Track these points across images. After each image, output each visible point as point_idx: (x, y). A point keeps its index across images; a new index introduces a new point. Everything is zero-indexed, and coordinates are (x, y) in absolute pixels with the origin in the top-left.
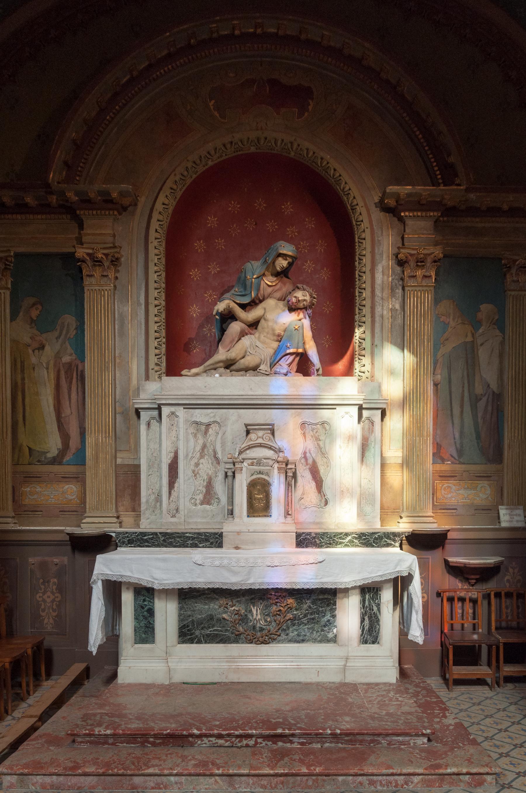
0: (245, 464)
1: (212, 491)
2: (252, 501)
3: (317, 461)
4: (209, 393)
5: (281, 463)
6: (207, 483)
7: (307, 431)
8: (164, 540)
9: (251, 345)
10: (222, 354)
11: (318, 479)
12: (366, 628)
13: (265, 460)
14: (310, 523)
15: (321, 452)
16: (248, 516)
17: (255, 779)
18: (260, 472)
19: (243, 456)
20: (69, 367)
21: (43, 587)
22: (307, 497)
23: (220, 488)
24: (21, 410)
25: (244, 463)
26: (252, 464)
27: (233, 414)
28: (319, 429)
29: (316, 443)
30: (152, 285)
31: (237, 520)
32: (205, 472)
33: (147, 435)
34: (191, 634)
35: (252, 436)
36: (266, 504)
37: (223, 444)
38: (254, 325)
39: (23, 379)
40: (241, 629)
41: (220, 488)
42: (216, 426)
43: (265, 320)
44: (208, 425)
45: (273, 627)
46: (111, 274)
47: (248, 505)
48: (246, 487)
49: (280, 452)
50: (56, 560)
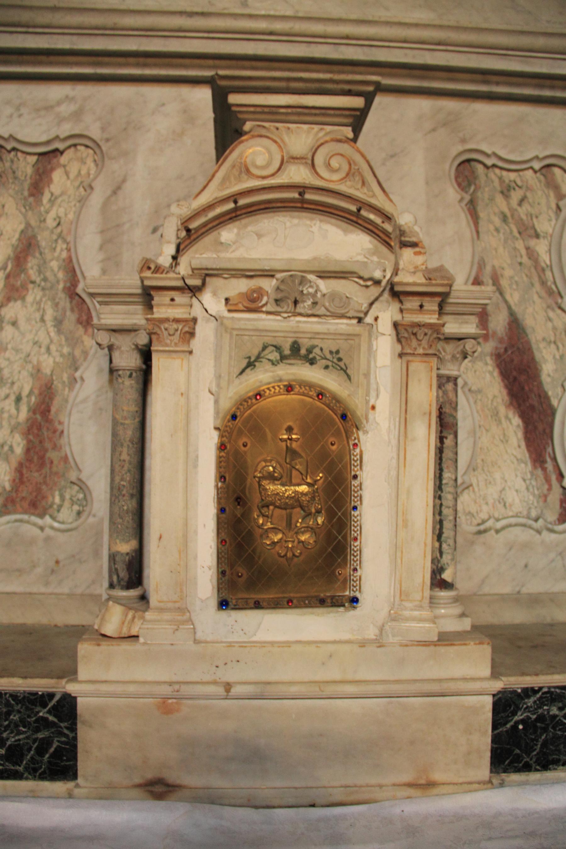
1: (56, 447)
2: (246, 514)
3: (528, 322)
5: (412, 303)
6: (33, 411)
7: (483, 195)
11: (534, 401)
13: (323, 286)
14: (503, 598)
15: (543, 283)
16: (223, 604)
18: (295, 348)
22: (488, 483)
25: (207, 297)
28: (529, 188)
29: (520, 245)
32: (27, 358)
36: (329, 537)
42: (83, 161)
47: (221, 542)
48: (214, 438)
49: (404, 245)
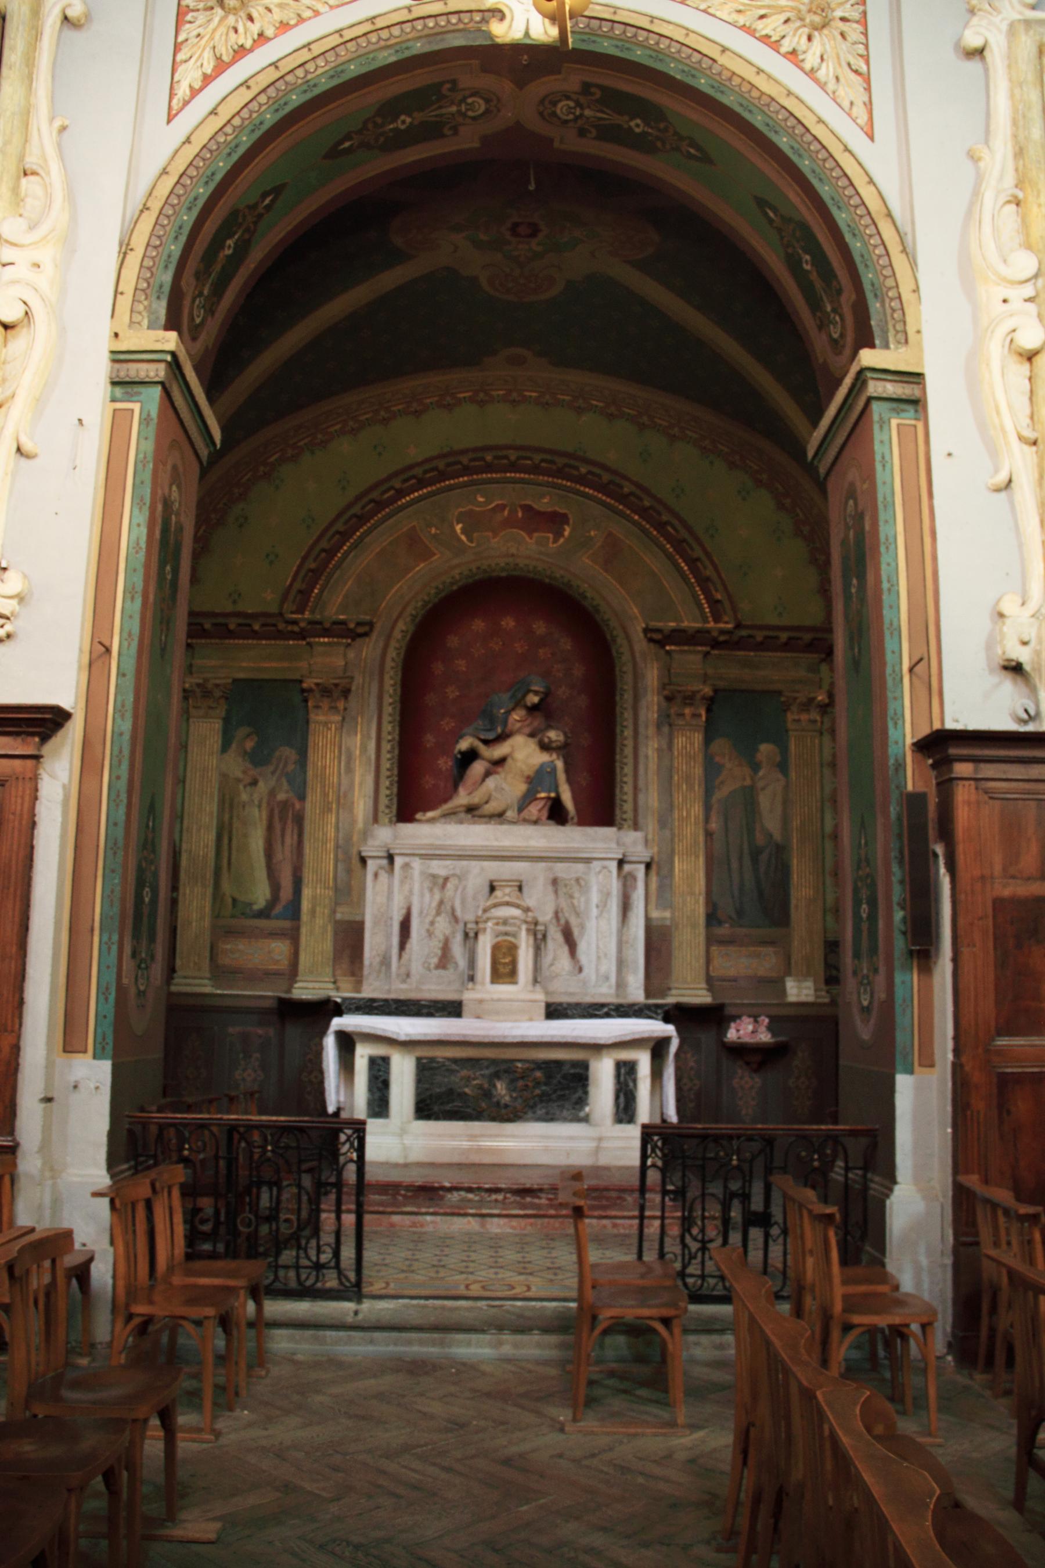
0: (490, 924)
4: (449, 842)
8: (396, 1008)
9: (496, 787)
10: (462, 798)
12: (622, 1106)
17: (506, 1220)
19: (488, 915)
20: (285, 805)
21: (242, 1062)
23: (458, 950)
24: (225, 854)
26: (497, 924)
27: (475, 866)
30: (386, 718)
31: (478, 987)
33: (374, 887)
34: (430, 1110)
35: (498, 893)
37: (463, 901)
38: (501, 762)
39: (231, 818)
40: (483, 1105)
41: (458, 950)
43: (513, 759)
44: (446, 879)
45: (519, 1104)
46: (341, 705)
50: (260, 1032)
